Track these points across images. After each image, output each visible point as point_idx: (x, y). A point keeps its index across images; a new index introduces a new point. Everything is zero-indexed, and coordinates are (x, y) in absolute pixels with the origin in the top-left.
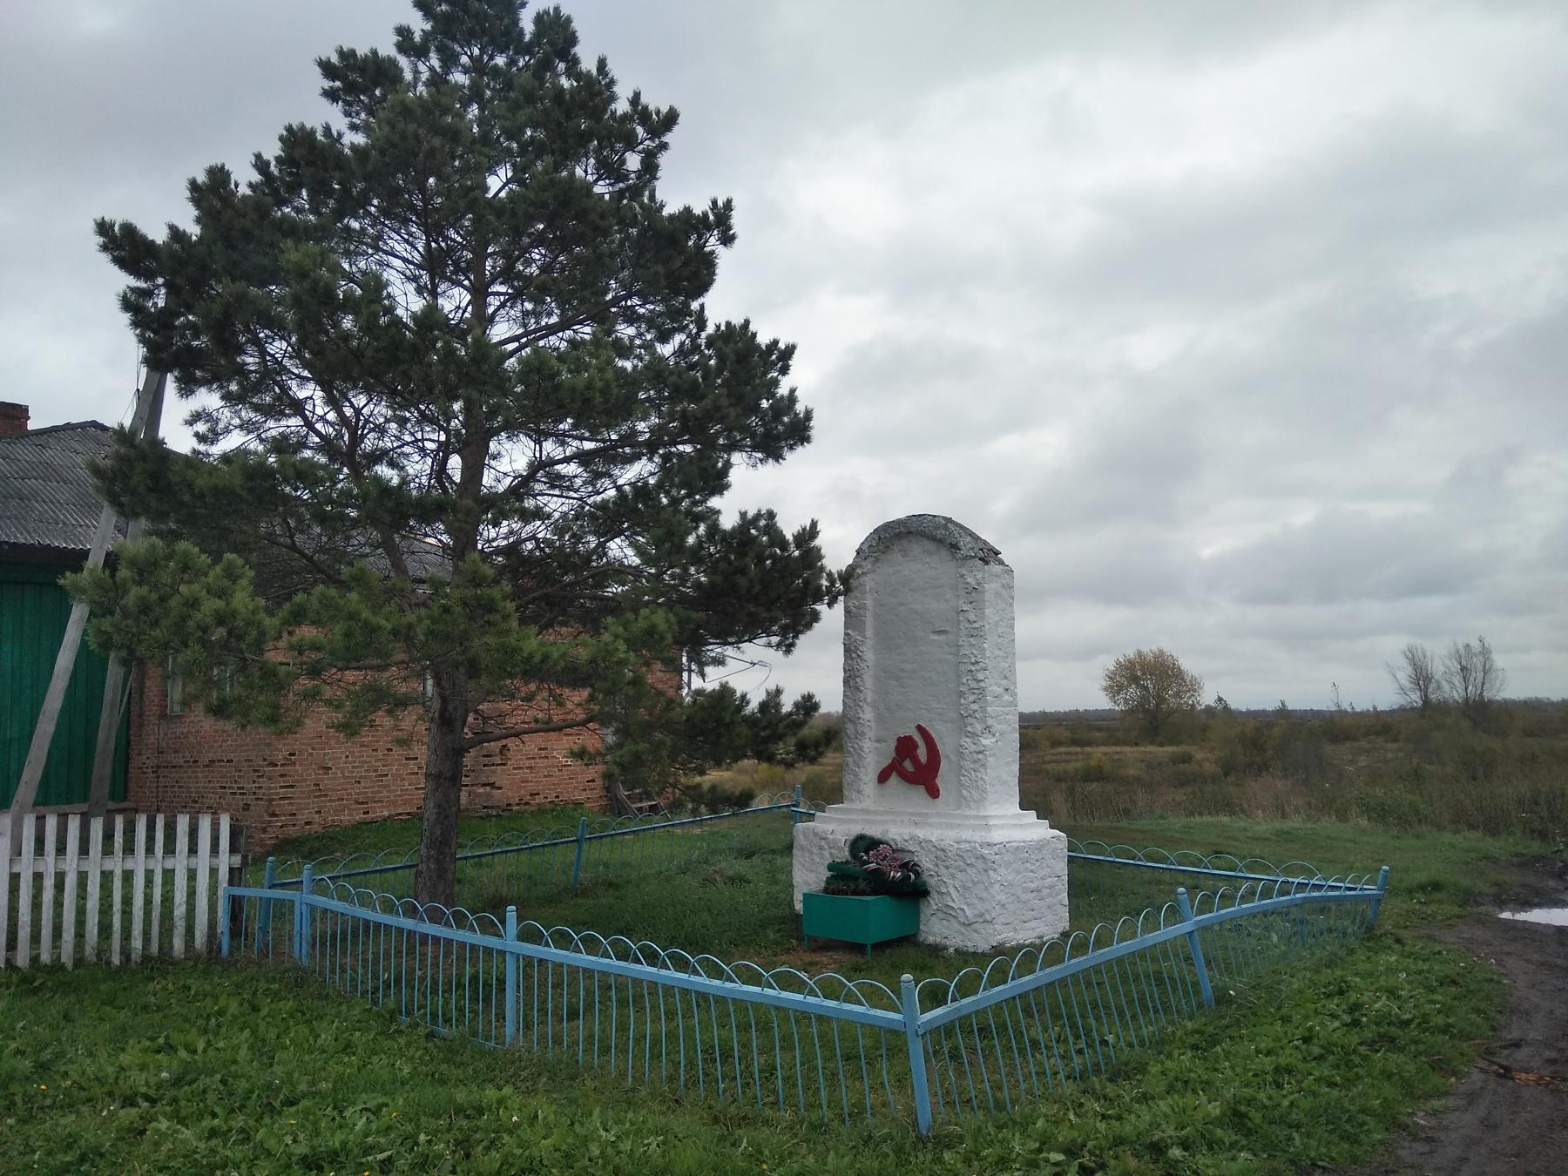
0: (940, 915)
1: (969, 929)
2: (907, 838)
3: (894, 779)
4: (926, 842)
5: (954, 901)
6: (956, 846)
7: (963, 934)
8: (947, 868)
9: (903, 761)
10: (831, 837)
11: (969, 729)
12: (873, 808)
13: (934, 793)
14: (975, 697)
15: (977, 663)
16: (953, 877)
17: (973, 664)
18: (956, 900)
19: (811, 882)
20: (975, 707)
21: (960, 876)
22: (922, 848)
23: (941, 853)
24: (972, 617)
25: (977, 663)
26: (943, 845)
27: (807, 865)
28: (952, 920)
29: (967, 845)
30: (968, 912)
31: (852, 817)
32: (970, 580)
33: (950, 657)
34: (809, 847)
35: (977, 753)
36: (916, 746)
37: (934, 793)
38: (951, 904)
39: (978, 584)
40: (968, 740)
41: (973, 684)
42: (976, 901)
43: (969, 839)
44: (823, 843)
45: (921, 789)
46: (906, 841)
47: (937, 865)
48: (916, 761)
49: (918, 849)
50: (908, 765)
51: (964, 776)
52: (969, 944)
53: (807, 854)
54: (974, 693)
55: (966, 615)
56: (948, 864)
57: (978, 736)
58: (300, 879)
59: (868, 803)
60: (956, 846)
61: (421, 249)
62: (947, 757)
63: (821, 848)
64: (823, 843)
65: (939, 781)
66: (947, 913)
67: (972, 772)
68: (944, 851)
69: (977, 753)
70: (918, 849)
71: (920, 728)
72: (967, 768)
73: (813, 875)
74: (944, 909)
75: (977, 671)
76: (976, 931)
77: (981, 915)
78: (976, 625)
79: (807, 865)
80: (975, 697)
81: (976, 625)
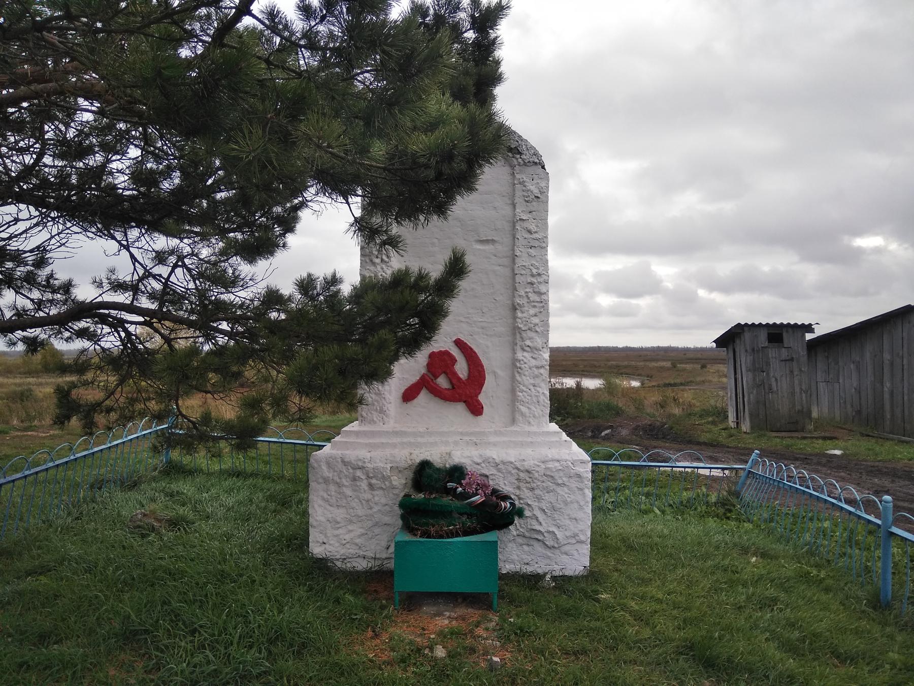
0: (520, 540)
1: (557, 552)
2: (479, 461)
3: (423, 397)
4: (504, 463)
5: (541, 524)
6: (543, 466)
7: (549, 558)
8: (532, 489)
9: (436, 377)
10: (369, 465)
11: (528, 343)
12: (398, 428)
13: (476, 409)
14: (537, 310)
15: (539, 275)
16: (539, 499)
17: (533, 276)
18: (543, 523)
19: (339, 519)
20: (536, 320)
21: (548, 497)
22: (499, 470)
23: (525, 475)
24: (533, 227)
25: (539, 275)
26: (527, 465)
27: (333, 501)
28: (535, 543)
29: (557, 464)
30: (559, 535)
31: (384, 440)
32: (532, 188)
33: (498, 268)
34: (336, 479)
35: (537, 368)
36: (454, 361)
37: (476, 409)
38: (538, 527)
39: (541, 193)
40: (525, 354)
41: (533, 297)
42: (568, 522)
43: (557, 457)
44: (359, 473)
45: (460, 408)
46: (478, 464)
47: (519, 488)
48: (452, 376)
49: (493, 471)
50: (442, 382)
51: (522, 391)
52: (556, 567)
53: (332, 488)
54: (534, 307)
55: (525, 225)
56: (534, 485)
57: (539, 350)
58: (455, 352)
59: (391, 425)
60: (543, 466)
61: (107, 402)
62: (494, 373)
63: (355, 479)
64: (359, 473)
65: (482, 398)
66: (534, 537)
67: (531, 387)
68: (528, 471)
69: (537, 368)
70: (493, 471)
71: (459, 343)
72: (526, 383)
73: (342, 511)
74: (527, 534)
75: (540, 283)
76: (566, 554)
77: (575, 536)
78: (536, 236)
79: (333, 501)
80: (537, 310)
81: (536, 236)
